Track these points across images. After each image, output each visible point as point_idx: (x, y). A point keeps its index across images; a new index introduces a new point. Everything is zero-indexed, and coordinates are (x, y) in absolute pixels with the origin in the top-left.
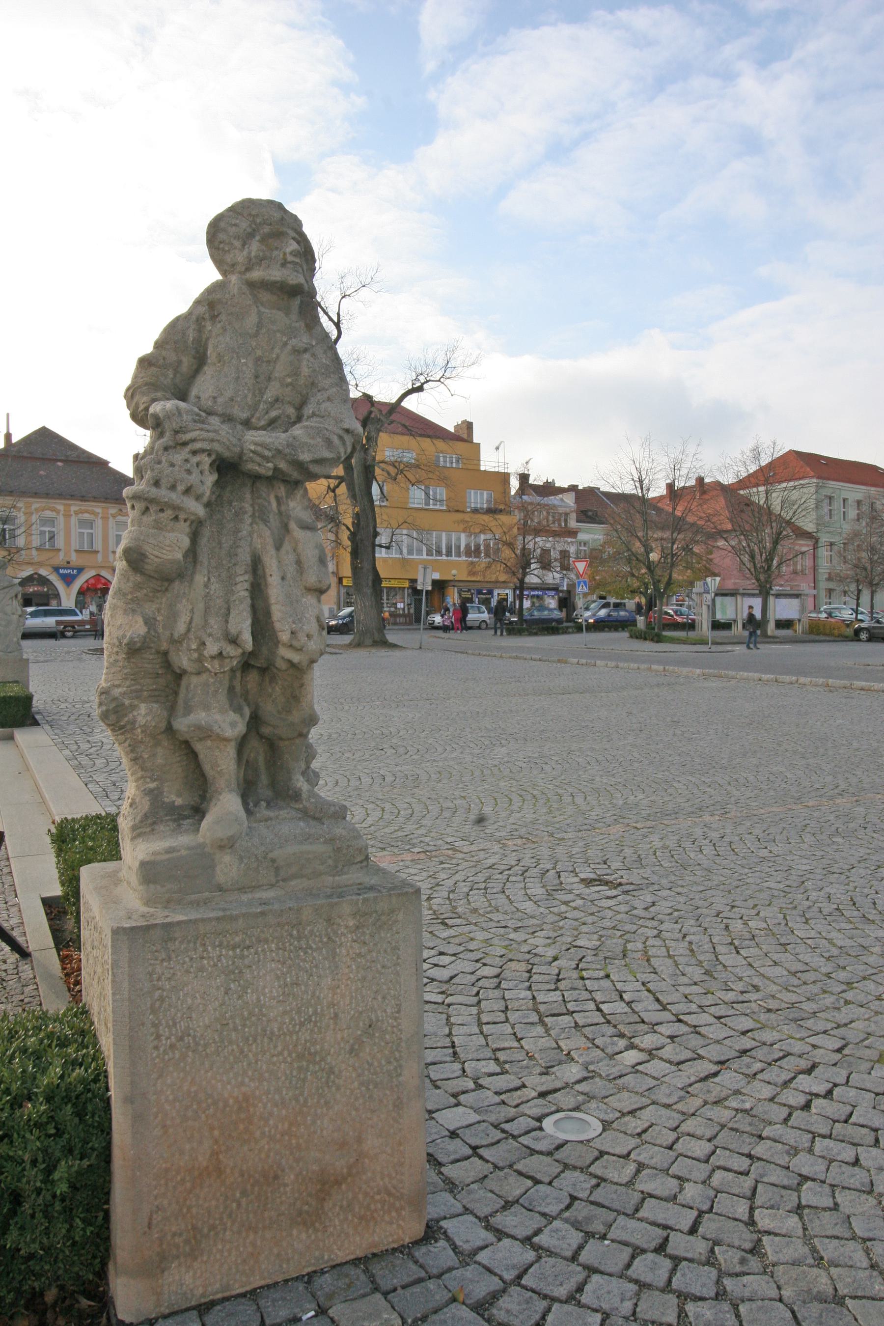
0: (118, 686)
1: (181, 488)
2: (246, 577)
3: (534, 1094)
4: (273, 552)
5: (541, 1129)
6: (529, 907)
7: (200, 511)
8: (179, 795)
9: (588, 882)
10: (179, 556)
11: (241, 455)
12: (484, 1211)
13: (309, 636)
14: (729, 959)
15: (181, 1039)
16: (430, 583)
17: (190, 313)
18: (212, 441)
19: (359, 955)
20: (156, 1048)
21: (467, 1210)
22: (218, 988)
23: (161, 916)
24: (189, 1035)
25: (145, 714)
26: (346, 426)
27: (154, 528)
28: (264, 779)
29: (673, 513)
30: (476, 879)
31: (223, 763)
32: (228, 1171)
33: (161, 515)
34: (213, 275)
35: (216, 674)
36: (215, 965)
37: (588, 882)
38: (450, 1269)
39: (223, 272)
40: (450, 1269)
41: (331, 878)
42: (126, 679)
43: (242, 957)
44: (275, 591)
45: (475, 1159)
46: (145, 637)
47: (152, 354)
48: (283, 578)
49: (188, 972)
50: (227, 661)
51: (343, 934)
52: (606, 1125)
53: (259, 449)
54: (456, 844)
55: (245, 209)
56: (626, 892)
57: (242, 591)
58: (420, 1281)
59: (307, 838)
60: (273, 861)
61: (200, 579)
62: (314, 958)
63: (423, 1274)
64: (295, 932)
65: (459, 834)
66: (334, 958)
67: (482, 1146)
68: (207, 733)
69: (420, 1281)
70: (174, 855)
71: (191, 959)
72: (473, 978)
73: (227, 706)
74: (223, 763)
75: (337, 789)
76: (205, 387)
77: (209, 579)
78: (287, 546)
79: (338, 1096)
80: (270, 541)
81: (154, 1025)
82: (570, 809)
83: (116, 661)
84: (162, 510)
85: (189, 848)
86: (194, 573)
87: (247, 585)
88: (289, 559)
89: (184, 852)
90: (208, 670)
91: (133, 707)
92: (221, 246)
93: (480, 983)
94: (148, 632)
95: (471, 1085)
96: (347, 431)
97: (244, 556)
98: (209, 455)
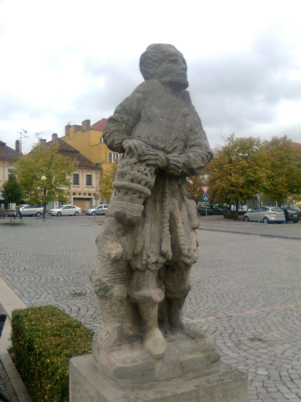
0: (106, 277)
1: (143, 183)
4: (179, 211)
7: (148, 191)
8: (131, 329)
11: (168, 165)
18: (156, 160)
25: (118, 290)
27: (130, 202)
28: (167, 319)
29: (244, 156)
33: (134, 195)
35: (153, 271)
37: (252, 340)
42: (110, 273)
46: (122, 254)
50: (159, 264)
53: (176, 163)
56: (271, 345)
59: (193, 351)
60: (181, 364)
61: (147, 225)
68: (148, 300)
78: (184, 208)
80: (177, 206)
82: (229, 301)
83: (105, 265)
84: (134, 193)
86: (144, 223)
88: (185, 213)
89: (140, 362)
90: (150, 269)
91: (112, 287)
92: (148, 65)
94: (123, 251)
98: (154, 167)
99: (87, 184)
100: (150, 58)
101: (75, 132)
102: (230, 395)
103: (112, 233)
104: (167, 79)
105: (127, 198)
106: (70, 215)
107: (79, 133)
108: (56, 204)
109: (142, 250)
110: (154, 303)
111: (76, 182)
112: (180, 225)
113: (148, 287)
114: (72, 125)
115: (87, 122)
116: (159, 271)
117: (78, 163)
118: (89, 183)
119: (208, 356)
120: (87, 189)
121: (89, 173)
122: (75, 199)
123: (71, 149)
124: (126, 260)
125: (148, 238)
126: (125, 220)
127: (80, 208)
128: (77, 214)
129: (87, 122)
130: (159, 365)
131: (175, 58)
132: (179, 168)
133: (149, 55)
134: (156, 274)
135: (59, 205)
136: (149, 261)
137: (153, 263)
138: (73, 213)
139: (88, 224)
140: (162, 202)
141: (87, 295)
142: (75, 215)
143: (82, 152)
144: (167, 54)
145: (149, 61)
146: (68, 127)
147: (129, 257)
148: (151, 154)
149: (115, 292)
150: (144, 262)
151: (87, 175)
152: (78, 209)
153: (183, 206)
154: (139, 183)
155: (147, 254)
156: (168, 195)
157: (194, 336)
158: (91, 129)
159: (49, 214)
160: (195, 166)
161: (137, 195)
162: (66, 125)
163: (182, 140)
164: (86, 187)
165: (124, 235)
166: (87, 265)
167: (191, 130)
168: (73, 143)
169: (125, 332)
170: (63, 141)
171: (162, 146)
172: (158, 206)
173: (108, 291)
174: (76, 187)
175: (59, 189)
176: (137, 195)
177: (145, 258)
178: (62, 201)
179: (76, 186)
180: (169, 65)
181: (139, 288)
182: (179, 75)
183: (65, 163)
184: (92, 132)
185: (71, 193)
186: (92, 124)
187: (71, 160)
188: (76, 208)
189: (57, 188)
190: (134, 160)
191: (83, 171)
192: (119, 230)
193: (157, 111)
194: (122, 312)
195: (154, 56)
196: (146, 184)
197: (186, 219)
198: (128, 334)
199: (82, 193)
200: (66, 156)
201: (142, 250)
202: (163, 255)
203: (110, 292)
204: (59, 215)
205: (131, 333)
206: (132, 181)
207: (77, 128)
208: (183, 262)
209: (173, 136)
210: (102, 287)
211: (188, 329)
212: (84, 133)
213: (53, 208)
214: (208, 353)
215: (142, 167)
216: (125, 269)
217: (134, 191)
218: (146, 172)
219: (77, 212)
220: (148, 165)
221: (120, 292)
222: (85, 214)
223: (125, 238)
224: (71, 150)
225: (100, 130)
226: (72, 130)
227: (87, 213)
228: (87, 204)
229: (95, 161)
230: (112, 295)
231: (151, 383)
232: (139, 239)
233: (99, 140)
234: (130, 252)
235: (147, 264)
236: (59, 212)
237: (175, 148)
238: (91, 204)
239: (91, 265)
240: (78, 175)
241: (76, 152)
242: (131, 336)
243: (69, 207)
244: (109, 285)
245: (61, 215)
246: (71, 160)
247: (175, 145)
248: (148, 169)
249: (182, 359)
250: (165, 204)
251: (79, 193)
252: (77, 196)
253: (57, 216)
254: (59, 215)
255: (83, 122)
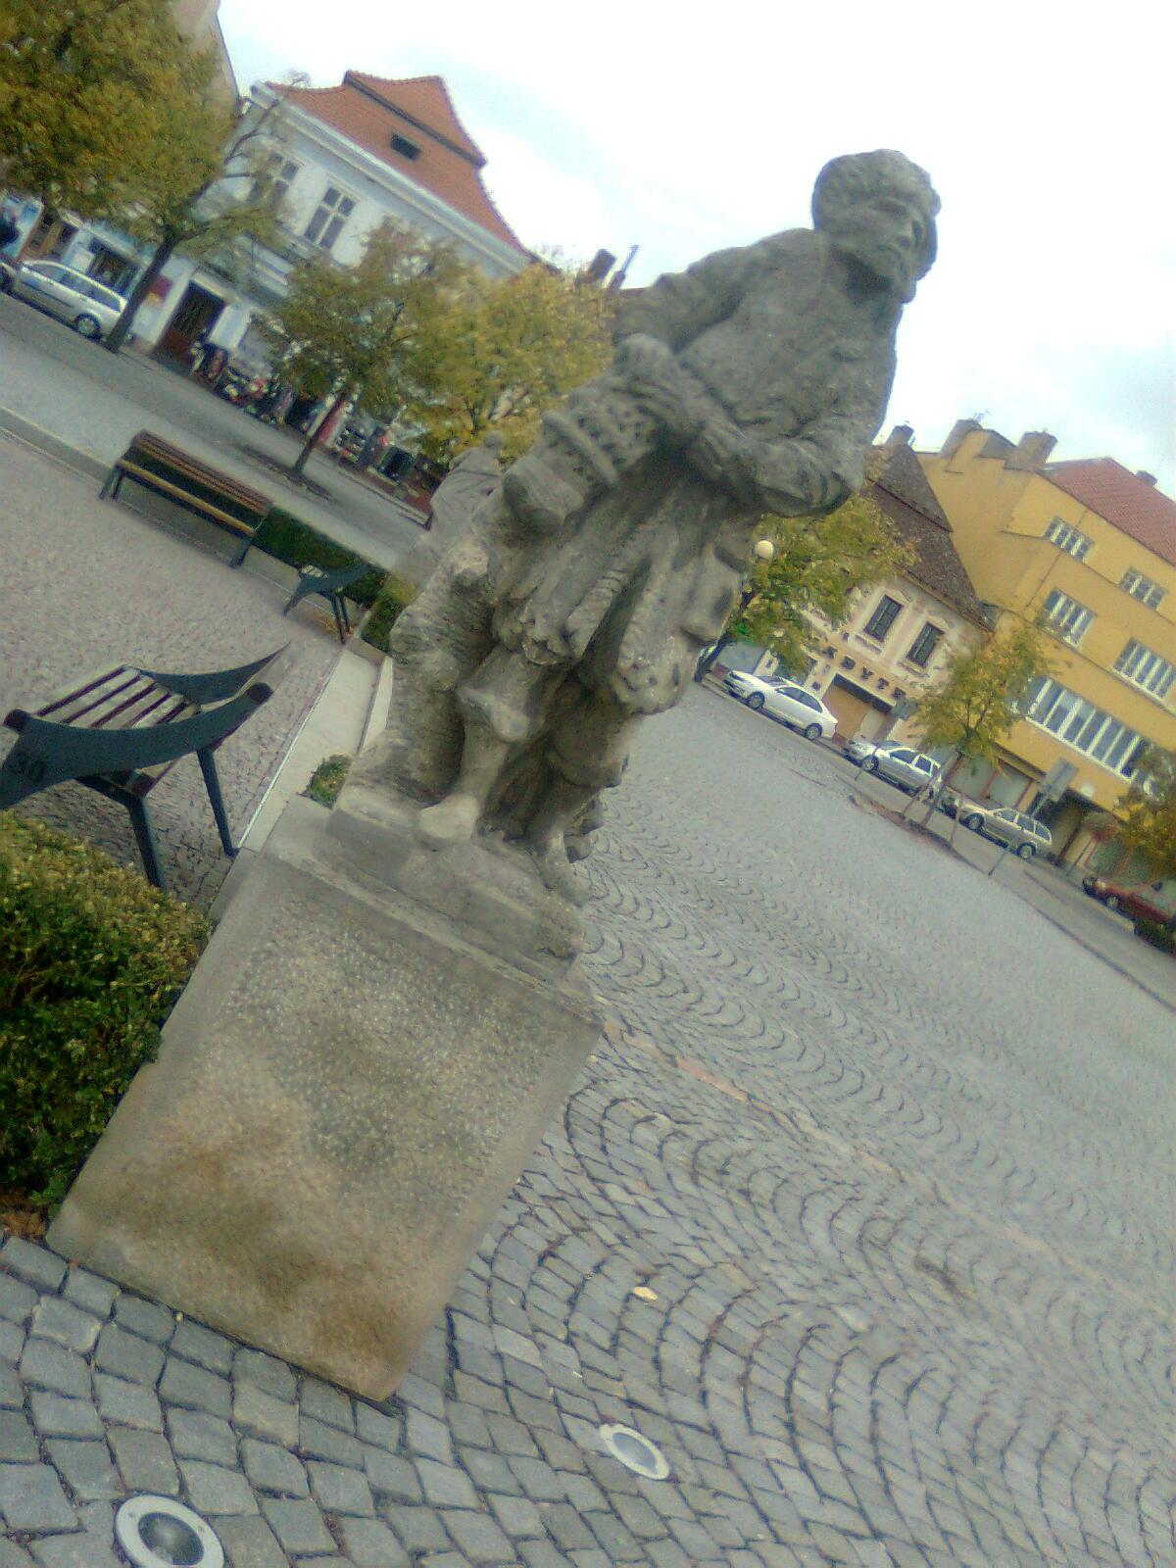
0: (426, 616)
1: (603, 440)
2: (621, 576)
3: (623, 1395)
4: (667, 565)
5: (597, 1427)
6: (820, 1237)
8: (422, 768)
9: (925, 1266)
10: (562, 513)
11: (695, 438)
12: (464, 1435)
13: (653, 681)
14: (1021, 1466)
15: (263, 1008)
16: (1061, 789)
17: (749, 251)
18: (668, 407)
19: (493, 1051)
20: (235, 999)
21: (446, 1421)
22: (330, 981)
23: (323, 870)
24: (273, 1008)
26: (839, 471)
30: (783, 1164)
31: (486, 762)
32: (229, 1174)
34: (808, 223)
36: (341, 956)
37: (925, 1266)
38: (381, 1447)
39: (817, 223)
40: (381, 1447)
41: (517, 954)
43: (374, 968)
44: (645, 611)
45: (499, 1392)
47: (677, 277)
48: (662, 601)
49: (311, 943)
50: (548, 655)
51: (488, 1015)
52: (673, 1480)
53: (714, 443)
54: (799, 1115)
55: (874, 163)
57: (606, 591)
58: (345, 1431)
59: (521, 898)
60: (469, 894)
61: (570, 551)
62: (444, 1020)
63: (351, 1428)
64: (441, 978)
65: (812, 1108)
66: (464, 1033)
67: (517, 1387)
68: (483, 719)
69: (345, 1431)
70: (375, 822)
71: (322, 933)
72: (673, 1250)
73: (522, 704)
74: (486, 762)
75: (712, 962)
76: (715, 345)
77: (581, 556)
78: (690, 569)
79: (382, 1183)
80: (671, 552)
81: (248, 976)
84: (570, 454)
85: (392, 825)
87: (615, 585)
88: (682, 582)
89: (384, 825)
91: (428, 647)
93: (674, 1260)
94: (487, 576)
95: (562, 1336)
96: (836, 477)
97: (632, 555)
99: (910, 656)
100: (840, 176)
101: (981, 456)
102: (527, 1028)
103: (486, 523)
104: (848, 244)
105: (550, 455)
106: (790, 726)
107: (993, 466)
108: (769, 664)
109: (526, 599)
110: (495, 739)
111: (879, 627)
112: (650, 597)
113: (500, 693)
114: (984, 427)
115: (1043, 442)
116: (549, 674)
117: (913, 559)
118: (919, 655)
119: (545, 931)
120: (901, 673)
121: (939, 622)
122: (839, 682)
123: (929, 505)
124: (485, 603)
125: (554, 579)
126: (522, 505)
127: (835, 721)
128: (812, 733)
129: (1043, 442)
130: (419, 858)
131: (901, 203)
132: (718, 460)
133: (843, 168)
134: (536, 677)
135: (775, 673)
136: (529, 633)
137: (535, 642)
138: (801, 724)
139: (813, 776)
140: (638, 520)
141: (599, 903)
142: (804, 733)
143: (957, 538)
144: (885, 183)
145: (836, 183)
146: (967, 429)
147: (494, 600)
148: (664, 389)
149: (428, 662)
150: (519, 629)
151: (929, 625)
152: (827, 719)
153: (691, 565)
154: (595, 435)
155: (532, 612)
156: (661, 514)
157: (552, 883)
158: (1041, 473)
159: (726, 682)
160: (764, 480)
161: (574, 461)
162: (966, 417)
163: (793, 410)
164: (900, 664)
165: (510, 543)
166: (684, 854)
167: (836, 402)
168: (949, 494)
169: (406, 767)
170: (919, 466)
171: (731, 396)
172: (624, 523)
173: (414, 650)
174: (865, 643)
175: (800, 615)
176: (574, 461)
177: (523, 619)
178: (791, 665)
179: (870, 640)
180: (874, 213)
181: (479, 685)
182: (879, 248)
183: (870, 538)
184: (1037, 484)
185: (839, 656)
186: (1056, 456)
187: (896, 539)
188: (820, 710)
189: (794, 607)
190: (618, 381)
191: (922, 603)
192: (502, 523)
193: (774, 310)
194: (423, 721)
195: (855, 176)
196: (608, 448)
197: (677, 596)
198: (408, 772)
199: (892, 686)
200: (886, 517)
201: (526, 599)
202: (566, 636)
203: (419, 656)
204: (755, 702)
205: (416, 775)
206: (582, 422)
207: (997, 445)
208: (610, 686)
209: (776, 389)
210: (410, 632)
211: (551, 862)
212: (1010, 473)
213: (752, 672)
214: (548, 924)
215: (623, 406)
216: (477, 626)
217: (573, 450)
218: (626, 421)
219: (818, 727)
220: (642, 410)
221: (438, 668)
222: (840, 750)
223: (508, 552)
224: (925, 510)
225: (1082, 502)
226: (975, 443)
227: (847, 750)
228: (871, 720)
229: (984, 591)
230: (419, 663)
231: (380, 882)
232: (536, 571)
233: (1047, 526)
234: (501, 586)
235: (521, 638)
236: (760, 695)
237: (761, 422)
238: (884, 730)
239: (695, 861)
240: (900, 607)
241: (941, 525)
242: (413, 782)
243: (802, 697)
244: (426, 638)
245: (760, 709)
246: (896, 539)
247: (764, 414)
248: (636, 418)
249: (479, 887)
250: (641, 527)
251: (865, 670)
252: (852, 677)
253: (747, 702)
254: (755, 702)
255: (1028, 437)
